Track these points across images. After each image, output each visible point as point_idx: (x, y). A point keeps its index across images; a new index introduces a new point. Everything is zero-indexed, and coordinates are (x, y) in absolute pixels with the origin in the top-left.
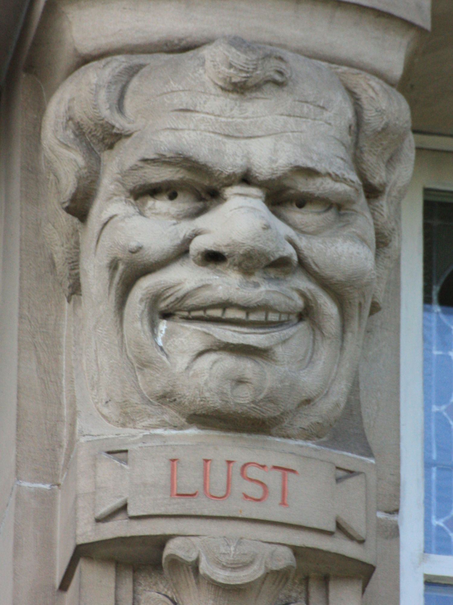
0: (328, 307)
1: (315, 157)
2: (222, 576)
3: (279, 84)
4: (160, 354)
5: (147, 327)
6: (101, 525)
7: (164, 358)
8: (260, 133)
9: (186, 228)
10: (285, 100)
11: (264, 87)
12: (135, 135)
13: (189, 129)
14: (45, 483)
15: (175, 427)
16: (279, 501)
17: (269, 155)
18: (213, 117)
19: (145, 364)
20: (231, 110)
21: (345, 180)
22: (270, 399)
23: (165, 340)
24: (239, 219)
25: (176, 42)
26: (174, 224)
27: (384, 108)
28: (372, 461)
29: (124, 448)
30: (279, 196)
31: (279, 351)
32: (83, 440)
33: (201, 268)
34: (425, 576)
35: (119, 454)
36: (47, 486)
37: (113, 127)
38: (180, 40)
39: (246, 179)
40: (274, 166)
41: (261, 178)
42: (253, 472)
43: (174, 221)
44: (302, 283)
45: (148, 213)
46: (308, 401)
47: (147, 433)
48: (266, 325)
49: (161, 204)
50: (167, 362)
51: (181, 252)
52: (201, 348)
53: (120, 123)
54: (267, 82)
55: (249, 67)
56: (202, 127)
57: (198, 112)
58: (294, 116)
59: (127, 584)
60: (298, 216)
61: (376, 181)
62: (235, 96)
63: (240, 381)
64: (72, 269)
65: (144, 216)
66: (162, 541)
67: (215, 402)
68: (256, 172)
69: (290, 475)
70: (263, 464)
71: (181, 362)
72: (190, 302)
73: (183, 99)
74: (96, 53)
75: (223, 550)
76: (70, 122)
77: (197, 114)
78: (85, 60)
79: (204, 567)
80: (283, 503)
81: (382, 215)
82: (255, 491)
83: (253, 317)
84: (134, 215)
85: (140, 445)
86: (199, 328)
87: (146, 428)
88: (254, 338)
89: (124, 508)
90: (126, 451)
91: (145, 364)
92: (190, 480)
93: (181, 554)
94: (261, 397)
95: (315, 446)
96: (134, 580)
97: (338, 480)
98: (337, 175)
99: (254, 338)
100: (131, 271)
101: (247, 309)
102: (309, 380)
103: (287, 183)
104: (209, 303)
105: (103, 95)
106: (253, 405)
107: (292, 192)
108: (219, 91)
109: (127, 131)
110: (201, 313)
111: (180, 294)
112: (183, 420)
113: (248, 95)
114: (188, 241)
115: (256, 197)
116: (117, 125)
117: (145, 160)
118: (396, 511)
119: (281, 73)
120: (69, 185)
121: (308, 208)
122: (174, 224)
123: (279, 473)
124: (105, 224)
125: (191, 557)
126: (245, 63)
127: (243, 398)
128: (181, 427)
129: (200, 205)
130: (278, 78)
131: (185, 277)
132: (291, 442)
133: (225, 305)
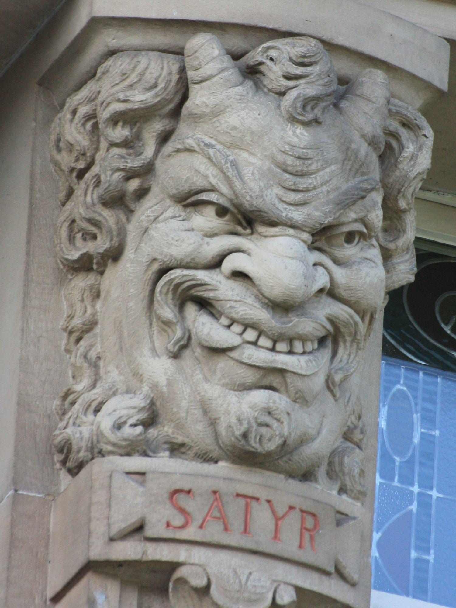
69: (254, 504)
123: (242, 502)
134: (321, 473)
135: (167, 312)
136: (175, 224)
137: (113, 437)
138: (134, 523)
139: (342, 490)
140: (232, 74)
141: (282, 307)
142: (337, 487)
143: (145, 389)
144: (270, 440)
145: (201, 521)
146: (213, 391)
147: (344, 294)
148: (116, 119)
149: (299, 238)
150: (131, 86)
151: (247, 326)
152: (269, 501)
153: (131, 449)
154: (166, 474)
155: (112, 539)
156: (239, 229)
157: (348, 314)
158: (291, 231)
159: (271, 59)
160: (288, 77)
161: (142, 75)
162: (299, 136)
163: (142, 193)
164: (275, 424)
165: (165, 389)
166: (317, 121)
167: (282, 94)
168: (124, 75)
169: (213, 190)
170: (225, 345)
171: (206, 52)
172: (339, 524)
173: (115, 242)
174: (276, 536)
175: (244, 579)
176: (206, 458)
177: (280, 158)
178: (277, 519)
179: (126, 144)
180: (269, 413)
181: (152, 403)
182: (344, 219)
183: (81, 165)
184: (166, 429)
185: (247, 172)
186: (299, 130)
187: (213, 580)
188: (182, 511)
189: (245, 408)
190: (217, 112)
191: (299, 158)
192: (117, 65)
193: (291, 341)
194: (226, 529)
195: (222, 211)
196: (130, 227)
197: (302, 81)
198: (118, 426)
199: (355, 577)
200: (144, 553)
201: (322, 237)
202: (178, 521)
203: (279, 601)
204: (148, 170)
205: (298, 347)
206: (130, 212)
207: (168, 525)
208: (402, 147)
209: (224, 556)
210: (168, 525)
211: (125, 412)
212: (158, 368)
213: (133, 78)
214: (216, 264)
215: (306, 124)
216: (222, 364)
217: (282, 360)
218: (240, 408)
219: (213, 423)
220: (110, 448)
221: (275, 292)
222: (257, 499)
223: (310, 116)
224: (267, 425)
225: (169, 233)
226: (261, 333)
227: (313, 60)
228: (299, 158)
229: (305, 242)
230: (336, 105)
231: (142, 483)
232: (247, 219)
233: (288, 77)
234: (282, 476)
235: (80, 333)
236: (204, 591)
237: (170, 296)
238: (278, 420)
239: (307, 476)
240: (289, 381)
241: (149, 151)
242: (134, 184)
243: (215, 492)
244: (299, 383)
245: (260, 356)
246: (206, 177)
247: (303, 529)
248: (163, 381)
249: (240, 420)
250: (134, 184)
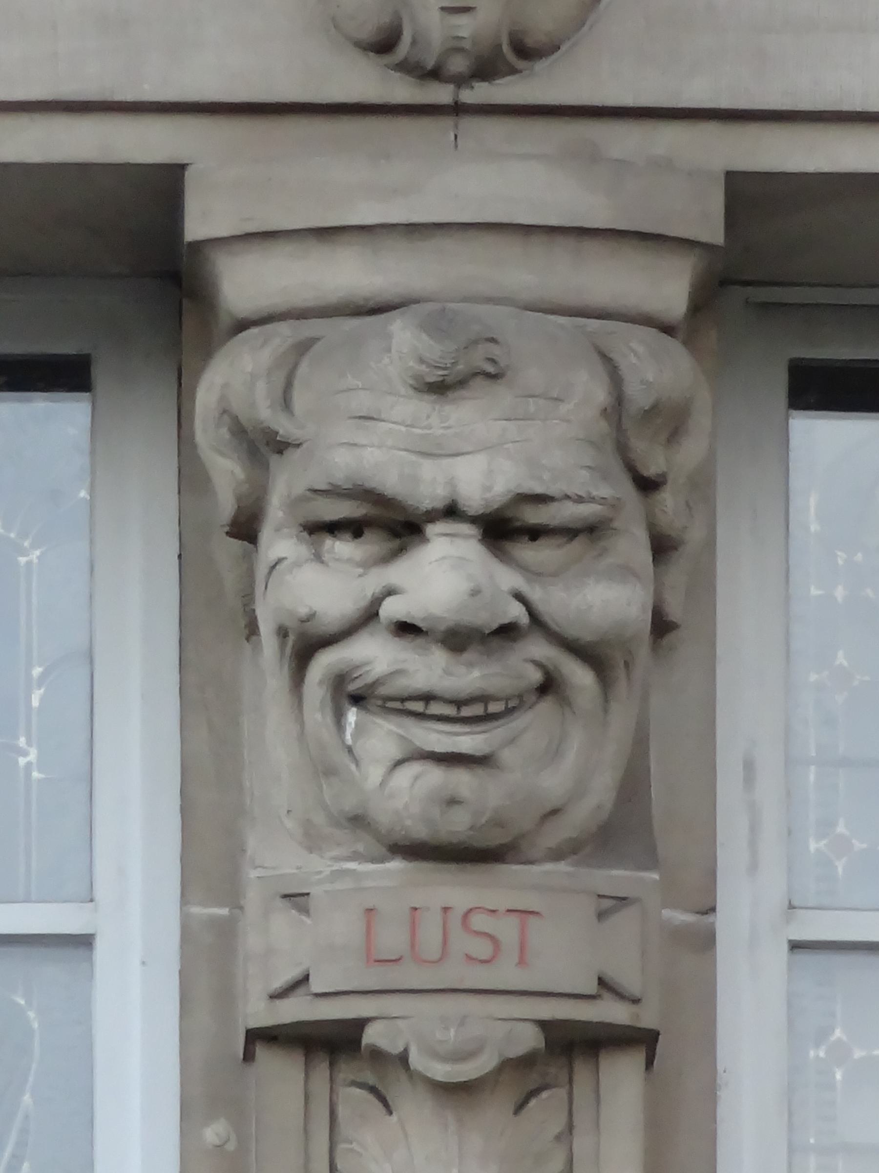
0: (579, 676)
1: (546, 476)
2: (441, 1071)
3: (493, 377)
4: (346, 759)
5: (329, 719)
6: (278, 1002)
7: (353, 767)
8: (470, 449)
9: (375, 581)
10: (502, 397)
11: (471, 383)
12: (305, 446)
13: (372, 446)
14: (221, 905)
15: (373, 860)
16: (516, 959)
17: (481, 478)
18: (403, 429)
19: (329, 771)
20: (428, 417)
21: (592, 500)
22: (497, 822)
23: (356, 734)
24: (443, 575)
25: (362, 303)
26: (360, 576)
27: (651, 380)
28: (656, 876)
29: (307, 891)
30: (500, 529)
31: (507, 756)
32: (253, 874)
33: (397, 639)
34: (790, 941)
35: (297, 899)
36: (224, 911)
37: (277, 433)
38: (367, 299)
39: (452, 511)
40: (488, 495)
41: (472, 512)
42: (479, 922)
43: (361, 570)
44: (539, 649)
45: (326, 557)
46: (555, 812)
47: (337, 866)
48: (487, 718)
49: (342, 548)
50: (357, 774)
51: (369, 616)
52: (398, 756)
53: (285, 427)
54: (475, 374)
55: (446, 362)
56: (390, 442)
57: (383, 421)
58: (516, 419)
59: (322, 1071)
60: (529, 553)
61: (651, 470)
62: (434, 397)
63: (453, 802)
64: (245, 605)
65: (322, 562)
66: (360, 1024)
67: (420, 832)
68: (464, 505)
69: (532, 919)
70: (492, 908)
71: (374, 774)
72: (383, 691)
73: (363, 402)
74: (255, 317)
75: (439, 1036)
76: (226, 417)
77: (383, 423)
78: (242, 325)
79: (416, 1060)
80: (522, 962)
81: (665, 512)
82: (483, 949)
83: (466, 712)
84: (307, 561)
85: (328, 887)
86: (393, 728)
87: (337, 859)
88: (467, 741)
89: (305, 979)
90: (308, 894)
91: (329, 771)
92: (392, 938)
93: (384, 1044)
94: (483, 821)
95: (570, 869)
96: (332, 1065)
97: (602, 915)
98: (580, 497)
99: (467, 741)
100: (306, 645)
101: (459, 703)
102: (554, 783)
103: (509, 514)
104: (406, 695)
105: (261, 387)
106: (472, 833)
107: (518, 524)
108: (411, 392)
109: (295, 440)
110: (397, 705)
111: (369, 679)
112: (384, 850)
113: (451, 395)
114: (377, 602)
115: (466, 537)
116: (281, 432)
117: (315, 491)
118: (713, 909)
119: (493, 361)
120: (226, 506)
121: (542, 542)
122: (360, 576)
123: (514, 919)
124: (273, 567)
125: (395, 1049)
126: (440, 358)
127: (457, 826)
128: (382, 860)
129: (396, 543)
130: (490, 369)
131: (374, 655)
132: (535, 868)
133: (428, 698)
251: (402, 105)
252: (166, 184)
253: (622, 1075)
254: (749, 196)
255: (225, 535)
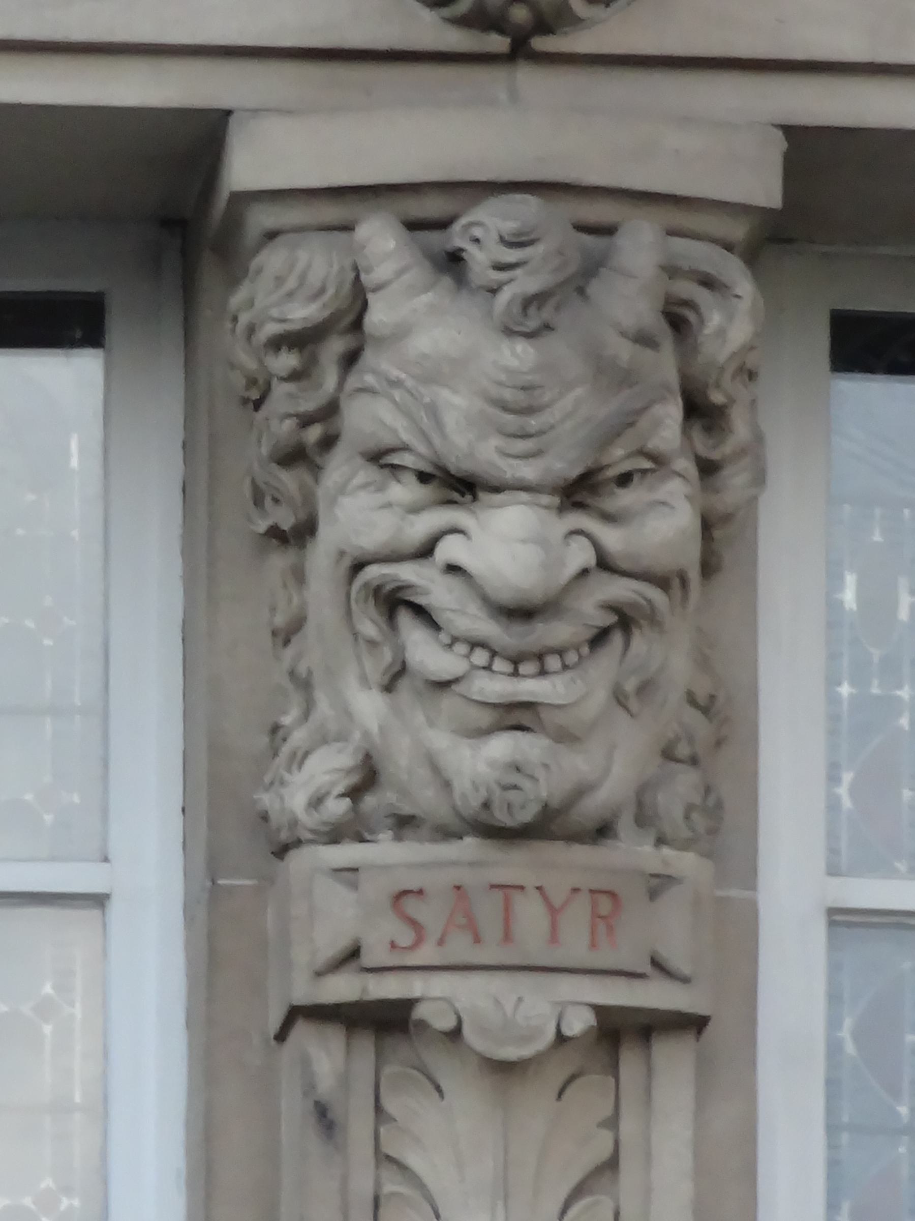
69: (517, 896)
123: (499, 895)
134: (625, 825)
135: (369, 628)
136: (365, 499)
137: (308, 820)
138: (900, 382)
139: (661, 841)
140: (419, 273)
141: (520, 613)
142: (652, 839)
143: (357, 735)
144: (523, 807)
145: (438, 935)
146: (440, 740)
147: (624, 565)
148: (277, 343)
149: (538, 505)
150: (290, 295)
151: (475, 644)
152: (539, 888)
153: (335, 835)
154: (386, 868)
155: (319, 974)
156: (456, 496)
157: (635, 592)
158: (524, 496)
159: (477, 241)
160: (501, 267)
161: (303, 278)
162: (519, 355)
163: (329, 442)
164: (526, 784)
165: (377, 740)
166: (547, 327)
167: (494, 291)
168: (280, 280)
169: (405, 448)
170: (446, 677)
171: (380, 240)
172: (653, 894)
173: (302, 516)
174: (554, 937)
175: (509, 1008)
176: (446, 834)
177: (495, 392)
178: (554, 911)
179: (295, 376)
180: (518, 769)
181: (368, 757)
182: (605, 461)
183: (255, 395)
184: (389, 794)
185: (450, 420)
186: (521, 346)
187: (465, 1018)
188: (414, 924)
189: (482, 768)
190: (401, 333)
191: (523, 388)
192: (272, 260)
193: (540, 657)
194: (477, 940)
195: (423, 477)
196: (321, 492)
197: (518, 272)
198: (317, 802)
199: (685, 969)
200: (364, 990)
201: (578, 492)
202: (406, 937)
203: (567, 1032)
204: (330, 411)
205: (553, 663)
206: (316, 470)
207: (393, 945)
208: (702, 321)
209: (477, 980)
210: (393, 945)
211: (327, 778)
212: (369, 706)
213: (291, 283)
214: (426, 551)
215: (529, 336)
216: (448, 702)
217: (530, 688)
218: (480, 763)
219: (447, 785)
220: (309, 836)
221: (505, 596)
222: (522, 888)
223: (532, 324)
224: (515, 787)
225: (362, 513)
226: (494, 654)
227: (532, 237)
228: (523, 388)
229: (546, 507)
230: (581, 291)
231: (354, 886)
232: (461, 486)
233: (501, 267)
234: (560, 844)
235: (286, 635)
236: (455, 1034)
237: (371, 602)
238: (532, 778)
239: (602, 831)
240: (542, 715)
241: (330, 379)
242: (314, 433)
243: (458, 888)
244: (560, 718)
245: (497, 686)
246: (394, 431)
247: (596, 916)
248: (374, 728)
249: (476, 787)
250: (314, 433)
251: (585, 55)
252: (203, 137)
253: (673, 1058)
254: (808, 149)
255: (683, 497)
